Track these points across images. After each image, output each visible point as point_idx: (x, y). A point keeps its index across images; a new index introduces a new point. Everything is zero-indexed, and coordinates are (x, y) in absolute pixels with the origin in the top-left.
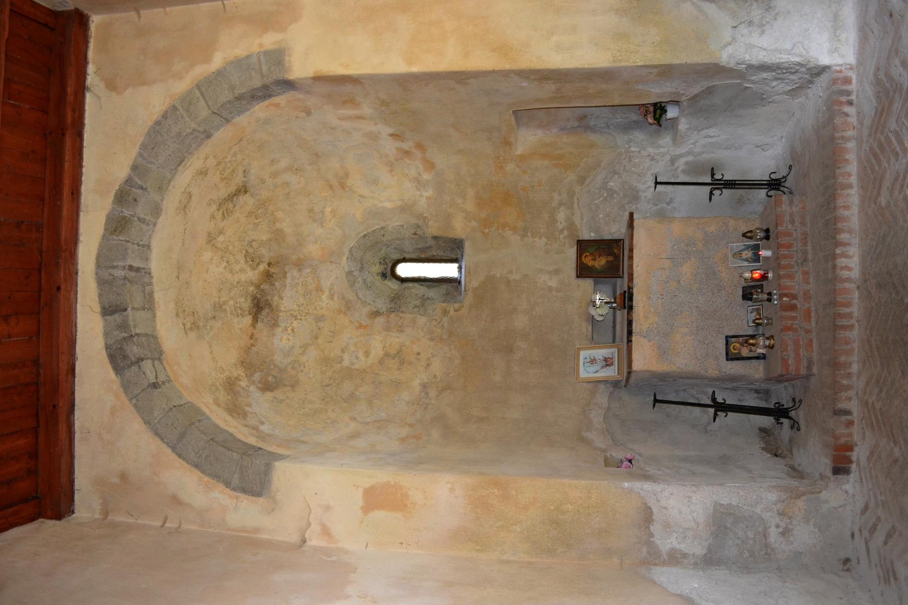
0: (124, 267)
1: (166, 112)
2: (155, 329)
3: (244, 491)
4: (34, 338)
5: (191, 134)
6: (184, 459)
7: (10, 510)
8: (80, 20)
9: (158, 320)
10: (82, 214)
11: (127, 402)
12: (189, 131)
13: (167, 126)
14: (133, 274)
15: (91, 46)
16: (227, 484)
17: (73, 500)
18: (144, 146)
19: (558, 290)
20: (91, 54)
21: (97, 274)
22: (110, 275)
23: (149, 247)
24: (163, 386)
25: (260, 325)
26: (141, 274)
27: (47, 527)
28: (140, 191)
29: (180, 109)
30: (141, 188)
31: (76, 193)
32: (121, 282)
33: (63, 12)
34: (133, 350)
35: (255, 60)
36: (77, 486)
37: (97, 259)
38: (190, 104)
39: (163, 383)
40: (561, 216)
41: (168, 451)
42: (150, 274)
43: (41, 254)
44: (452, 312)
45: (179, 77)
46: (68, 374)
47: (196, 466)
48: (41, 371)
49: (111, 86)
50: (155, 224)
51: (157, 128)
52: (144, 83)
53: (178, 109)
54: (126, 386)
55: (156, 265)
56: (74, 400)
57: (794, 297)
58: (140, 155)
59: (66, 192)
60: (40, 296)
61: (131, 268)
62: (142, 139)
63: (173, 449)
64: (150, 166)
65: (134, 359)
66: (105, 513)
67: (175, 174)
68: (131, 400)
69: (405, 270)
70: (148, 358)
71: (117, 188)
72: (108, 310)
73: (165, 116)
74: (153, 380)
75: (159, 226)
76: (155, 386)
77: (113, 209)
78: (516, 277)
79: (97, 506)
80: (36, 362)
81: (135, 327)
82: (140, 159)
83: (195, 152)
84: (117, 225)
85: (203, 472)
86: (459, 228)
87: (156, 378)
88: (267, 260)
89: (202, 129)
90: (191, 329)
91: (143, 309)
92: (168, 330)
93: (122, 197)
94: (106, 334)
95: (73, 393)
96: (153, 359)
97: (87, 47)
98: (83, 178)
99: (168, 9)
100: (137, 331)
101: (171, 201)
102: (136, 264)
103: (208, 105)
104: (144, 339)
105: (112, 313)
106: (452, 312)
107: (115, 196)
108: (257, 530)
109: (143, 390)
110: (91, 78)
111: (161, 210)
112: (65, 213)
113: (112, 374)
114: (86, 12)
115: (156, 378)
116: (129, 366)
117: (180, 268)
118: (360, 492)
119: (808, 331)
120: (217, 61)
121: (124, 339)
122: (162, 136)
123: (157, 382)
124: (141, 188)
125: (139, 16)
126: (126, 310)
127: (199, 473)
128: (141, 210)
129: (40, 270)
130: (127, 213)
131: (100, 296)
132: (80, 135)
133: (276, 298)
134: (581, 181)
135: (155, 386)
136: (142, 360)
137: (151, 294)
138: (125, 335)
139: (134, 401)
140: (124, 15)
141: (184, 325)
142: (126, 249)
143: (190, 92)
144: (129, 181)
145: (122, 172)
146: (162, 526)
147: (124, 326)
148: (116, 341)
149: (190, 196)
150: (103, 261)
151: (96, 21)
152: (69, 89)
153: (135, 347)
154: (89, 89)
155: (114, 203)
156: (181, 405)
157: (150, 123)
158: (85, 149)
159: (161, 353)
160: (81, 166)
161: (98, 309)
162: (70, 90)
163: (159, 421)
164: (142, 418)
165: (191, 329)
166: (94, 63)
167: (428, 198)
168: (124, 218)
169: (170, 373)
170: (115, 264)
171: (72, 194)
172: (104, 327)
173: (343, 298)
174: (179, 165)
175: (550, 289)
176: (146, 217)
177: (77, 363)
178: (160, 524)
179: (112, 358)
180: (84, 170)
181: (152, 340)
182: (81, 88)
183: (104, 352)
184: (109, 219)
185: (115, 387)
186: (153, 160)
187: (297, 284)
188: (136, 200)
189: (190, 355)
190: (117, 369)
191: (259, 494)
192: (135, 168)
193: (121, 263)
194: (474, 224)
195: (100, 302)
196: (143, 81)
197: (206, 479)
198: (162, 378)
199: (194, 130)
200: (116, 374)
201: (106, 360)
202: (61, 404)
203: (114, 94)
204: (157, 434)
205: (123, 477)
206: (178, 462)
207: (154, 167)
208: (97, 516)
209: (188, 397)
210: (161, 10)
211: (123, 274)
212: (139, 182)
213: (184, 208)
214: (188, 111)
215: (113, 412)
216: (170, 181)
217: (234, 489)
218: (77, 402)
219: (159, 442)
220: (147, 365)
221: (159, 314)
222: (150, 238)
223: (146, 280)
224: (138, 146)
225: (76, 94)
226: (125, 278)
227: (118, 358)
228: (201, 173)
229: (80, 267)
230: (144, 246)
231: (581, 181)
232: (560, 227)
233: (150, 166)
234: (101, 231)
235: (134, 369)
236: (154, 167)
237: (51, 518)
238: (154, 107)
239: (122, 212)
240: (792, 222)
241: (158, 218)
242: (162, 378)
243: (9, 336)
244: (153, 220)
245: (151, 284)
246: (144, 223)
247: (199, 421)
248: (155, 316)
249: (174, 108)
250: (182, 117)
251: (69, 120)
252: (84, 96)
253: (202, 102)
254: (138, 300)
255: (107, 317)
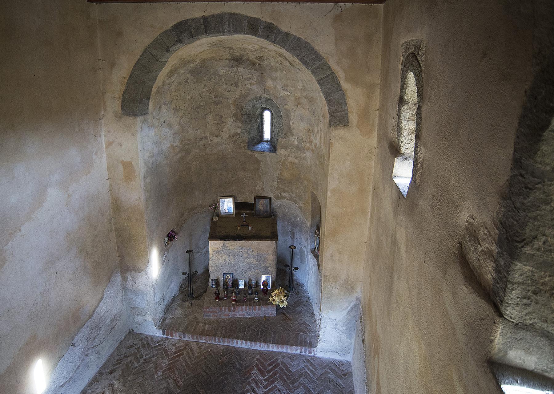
3: (123, 102)
16: (125, 92)
18: (299, 40)
19: (255, 189)
21: (225, 14)
25: (228, 61)
35: (344, 107)
40: (286, 194)
44: (243, 145)
47: (131, 76)
57: (234, 311)
63: (137, 62)
69: (267, 115)
72: (205, 20)
73: (316, 53)
78: (260, 172)
86: (281, 152)
88: (261, 63)
103: (321, 79)
105: (204, 24)
106: (243, 145)
108: (105, 109)
113: (171, 25)
118: (130, 160)
119: (220, 315)
120: (345, 85)
121: (191, 32)
133: (244, 66)
134: (299, 207)
138: (193, 32)
143: (329, 68)
144: (280, 32)
167: (294, 141)
172: (197, 18)
173: (248, 94)
175: (255, 186)
179: (180, 24)
187: (252, 75)
188: (268, 37)
191: (122, 109)
192: (287, 35)
194: (283, 159)
195: (210, 16)
197: (126, 81)
212: (278, 39)
217: (123, 96)
219: (141, 54)
231: (299, 207)
232: (282, 193)
233: (288, 45)
234: (250, 15)
240: (265, 311)
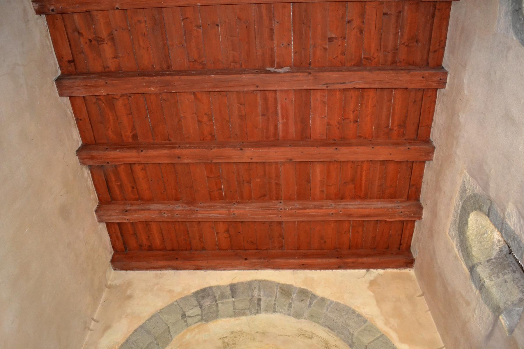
0: (259, 295)
1: (362, 316)
2: (222, 317)
4: (217, 247)
5: (350, 333)
6: (133, 333)
7: (119, 235)
8: (409, 263)
9: (228, 319)
10: (291, 271)
11: (175, 299)
12: (351, 331)
13: (353, 317)
14: (256, 301)
15: (395, 271)
17: (121, 270)
18: (337, 304)
20: (390, 271)
21: (256, 280)
22: (255, 288)
23: (275, 311)
24: (183, 321)
26: (256, 306)
27: (108, 253)
28: (308, 303)
29: (365, 325)
30: (311, 304)
31: (304, 267)
32: (250, 294)
33: (411, 253)
34: (207, 302)
36: (128, 272)
37: (264, 280)
38: (369, 331)
39: (186, 321)
41: (140, 324)
42: (258, 313)
43: (266, 249)
45: (387, 323)
46: (195, 266)
47: (127, 341)
48: (198, 252)
49: (372, 283)
50: (289, 315)
51: (351, 311)
52: (378, 301)
53: (364, 323)
54: (185, 299)
55: (263, 317)
56: (181, 270)
58: (332, 302)
59: (304, 261)
60: (242, 250)
61: (259, 300)
62: (342, 303)
63: (141, 327)
64: (325, 308)
65: (202, 302)
66: (110, 287)
67: (322, 325)
68: (177, 301)
70: (202, 311)
71: (309, 290)
72: (233, 288)
73: (359, 316)
74: (187, 314)
75: (289, 318)
76: (184, 316)
77: (296, 288)
79: (117, 282)
80: (203, 249)
81: (222, 303)
82: (329, 302)
83: (339, 338)
84: (286, 291)
85: (122, 346)
87: (189, 317)
89: (354, 340)
90: (224, 342)
91: (234, 309)
92: (222, 326)
93: (304, 293)
94: (218, 287)
95: (184, 269)
96: (201, 315)
97: (393, 268)
98: (313, 271)
99: (429, 312)
100: (220, 305)
101: (305, 325)
102: (262, 304)
104: (215, 309)
107: (305, 289)
109: (182, 308)
110: (375, 272)
111: (299, 318)
112: (291, 261)
113: (194, 290)
114: (414, 266)
115: (189, 317)
116: (197, 300)
117: (264, 334)
121: (215, 297)
122: (346, 314)
123: (186, 317)
124: (311, 304)
125: (420, 296)
126: (233, 297)
127: (122, 342)
128: (296, 304)
129: (257, 249)
130: (294, 296)
131: (242, 283)
132: (339, 267)
135: (184, 316)
136: (201, 308)
137: (244, 314)
139: (175, 303)
140: (419, 287)
141: (226, 337)
142: (271, 296)
144: (314, 296)
145: (319, 292)
146: (93, 319)
147: (223, 296)
148: (214, 293)
149: (311, 338)
150: (263, 284)
151: (411, 272)
152: (365, 259)
153: (209, 303)
154: (368, 271)
155: (300, 289)
156: (170, 332)
157: (353, 307)
158: (331, 271)
159: (207, 321)
160: (321, 269)
161: (234, 282)
162: (365, 260)
163: (160, 318)
164: (164, 308)
165: (224, 342)
166: (385, 273)
168: (291, 295)
169: (193, 326)
170: (262, 290)
171: (303, 265)
172: (223, 286)
174: (329, 328)
176: (293, 308)
177: (202, 271)
178: (95, 318)
179: (204, 290)
180: (319, 271)
181: (214, 315)
182: (368, 266)
183: (208, 286)
184: (290, 286)
185: (186, 292)
186: (329, 310)
188: (302, 301)
189: (206, 341)
190: (196, 294)
192: (323, 300)
193: (262, 293)
195: (238, 283)
196: (380, 301)
198: (189, 320)
199: (353, 335)
200: (194, 293)
201: (203, 287)
202: (178, 262)
203: (368, 285)
204: (152, 317)
205: (130, 297)
206: (132, 330)
207: (325, 311)
208: (109, 282)
209: (176, 338)
210: (428, 308)
211: (255, 295)
212: (314, 302)
213: (302, 334)
214: (365, 330)
215: (170, 291)
216: (318, 322)
218: (178, 271)
219: (147, 318)
220: (197, 311)
221: (232, 320)
222: (281, 312)
223: (253, 311)
224: (337, 301)
225: (364, 263)
226: (253, 296)
227: (203, 294)
228: (326, 344)
229: (260, 271)
230: (274, 308)
233: (325, 308)
235: (196, 303)
236: (325, 311)
237: (113, 258)
238: (364, 309)
239: (294, 293)
241: (294, 316)
242: (189, 320)
243: (217, 233)
244: (292, 313)
245: (251, 314)
246: (289, 307)
247: (158, 344)
248: (231, 317)
249: (365, 321)
250: (360, 327)
251: (347, 260)
252: (363, 268)
253: (372, 339)
254: (240, 306)
255: (229, 288)
